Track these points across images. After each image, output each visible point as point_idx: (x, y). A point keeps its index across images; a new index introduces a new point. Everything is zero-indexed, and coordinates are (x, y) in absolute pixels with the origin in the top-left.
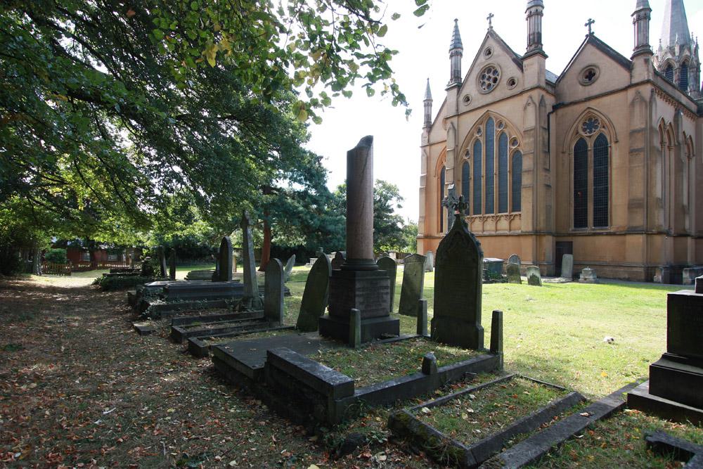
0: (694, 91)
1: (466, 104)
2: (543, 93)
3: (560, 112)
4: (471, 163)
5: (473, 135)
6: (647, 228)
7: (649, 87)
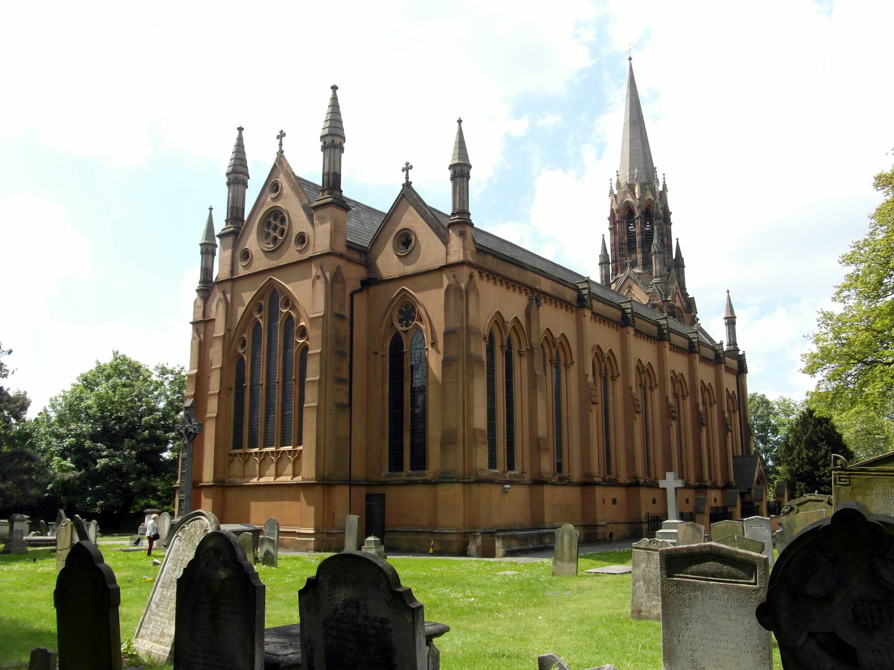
0: (659, 252)
2: (341, 263)
3: (373, 290)
6: (464, 473)
7: (466, 271)
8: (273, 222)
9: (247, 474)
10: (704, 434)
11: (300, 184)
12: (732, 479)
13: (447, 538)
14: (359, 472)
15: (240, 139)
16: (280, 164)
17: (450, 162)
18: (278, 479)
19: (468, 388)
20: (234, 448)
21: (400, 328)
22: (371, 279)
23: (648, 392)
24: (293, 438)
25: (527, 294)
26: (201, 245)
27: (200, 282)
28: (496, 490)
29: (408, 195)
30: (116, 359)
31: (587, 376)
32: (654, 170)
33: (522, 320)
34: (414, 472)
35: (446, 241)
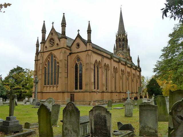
1: (46, 49)
2: (66, 49)
3: (72, 55)
4: (47, 68)
5: (47, 59)
7: (90, 52)
10: (133, 83)
11: (57, 33)
12: (138, 91)
13: (86, 102)
14: (69, 91)
15: (44, 23)
16: (53, 29)
23: (108, 71)
24: (57, 84)
28: (95, 93)
29: (79, 36)
32: (125, 31)
35: (86, 46)
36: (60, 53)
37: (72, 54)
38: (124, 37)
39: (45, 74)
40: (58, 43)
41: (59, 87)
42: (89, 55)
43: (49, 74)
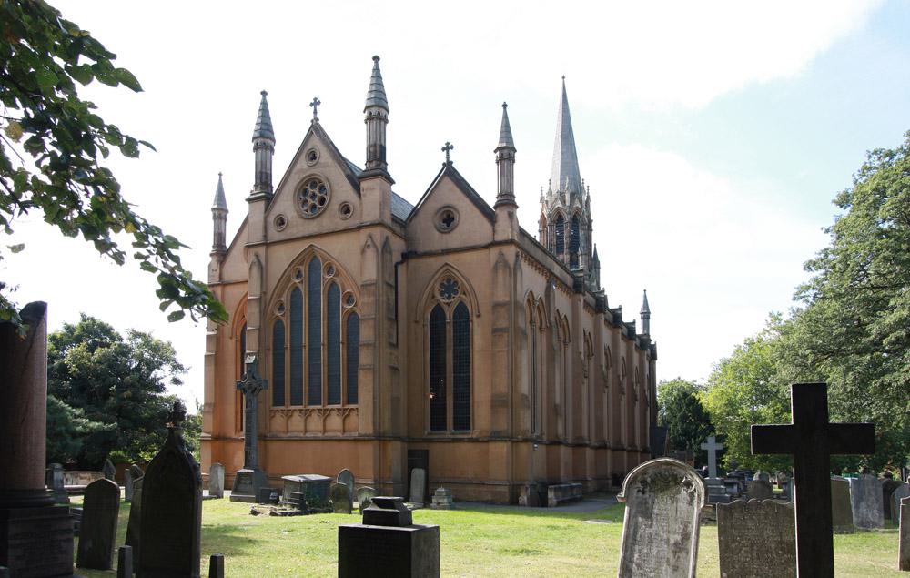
2: (389, 233)
3: (413, 263)
5: (289, 280)
8: (311, 190)
9: (290, 429)
17: (496, 144)
18: (326, 434)
19: (516, 358)
20: (275, 404)
21: (443, 301)
22: (411, 252)
25: (546, 276)
26: (213, 210)
27: (213, 247)
30: (84, 320)
31: (581, 353)
33: (544, 299)
34: (457, 431)
36: (363, 252)
37: (412, 258)
38: (560, 205)
39: (275, 349)
40: (348, 199)
41: (353, 419)
42: (506, 264)
43: (296, 350)
